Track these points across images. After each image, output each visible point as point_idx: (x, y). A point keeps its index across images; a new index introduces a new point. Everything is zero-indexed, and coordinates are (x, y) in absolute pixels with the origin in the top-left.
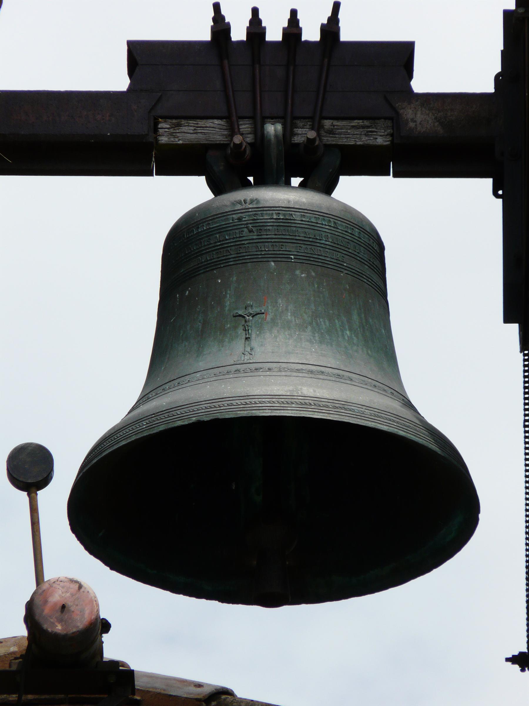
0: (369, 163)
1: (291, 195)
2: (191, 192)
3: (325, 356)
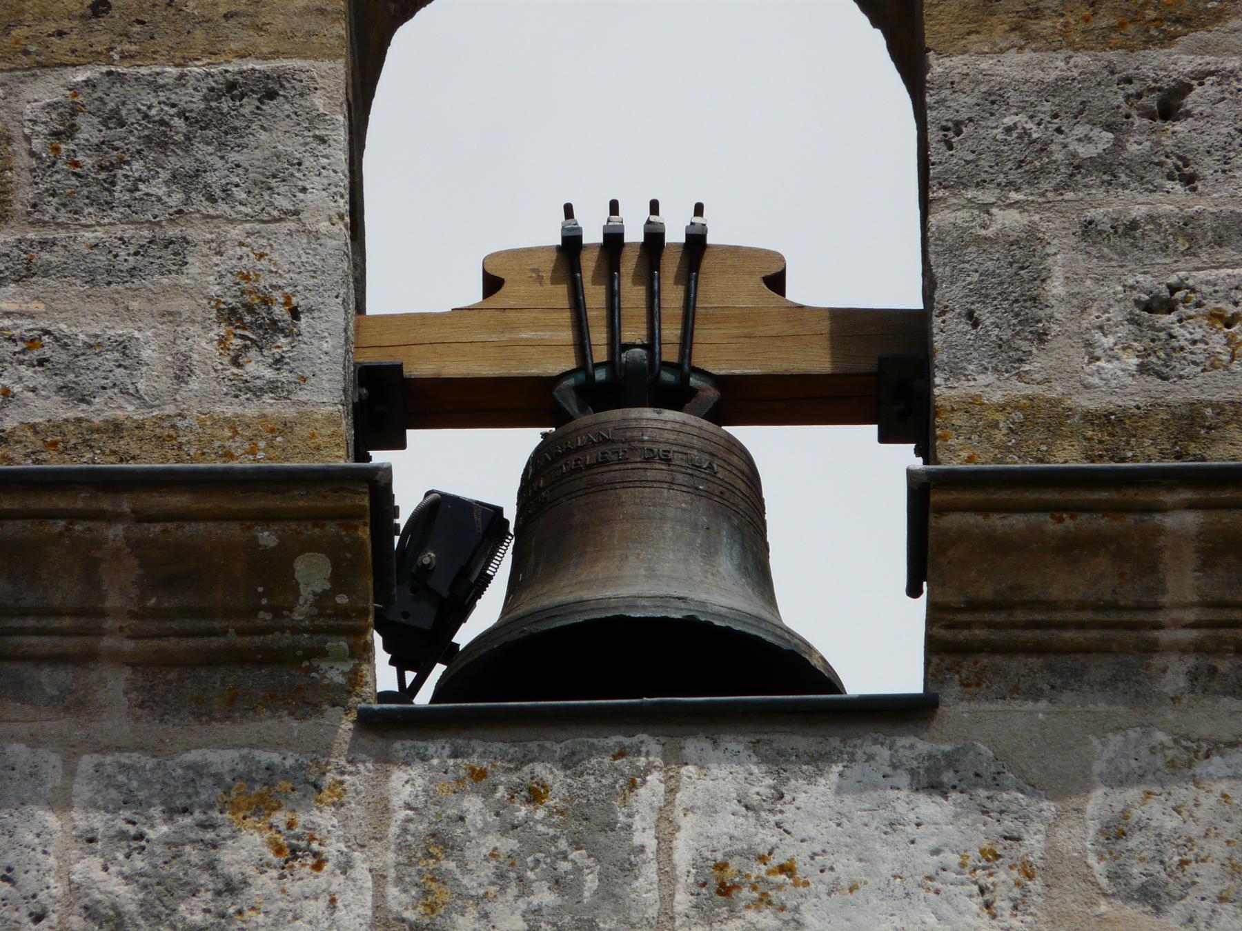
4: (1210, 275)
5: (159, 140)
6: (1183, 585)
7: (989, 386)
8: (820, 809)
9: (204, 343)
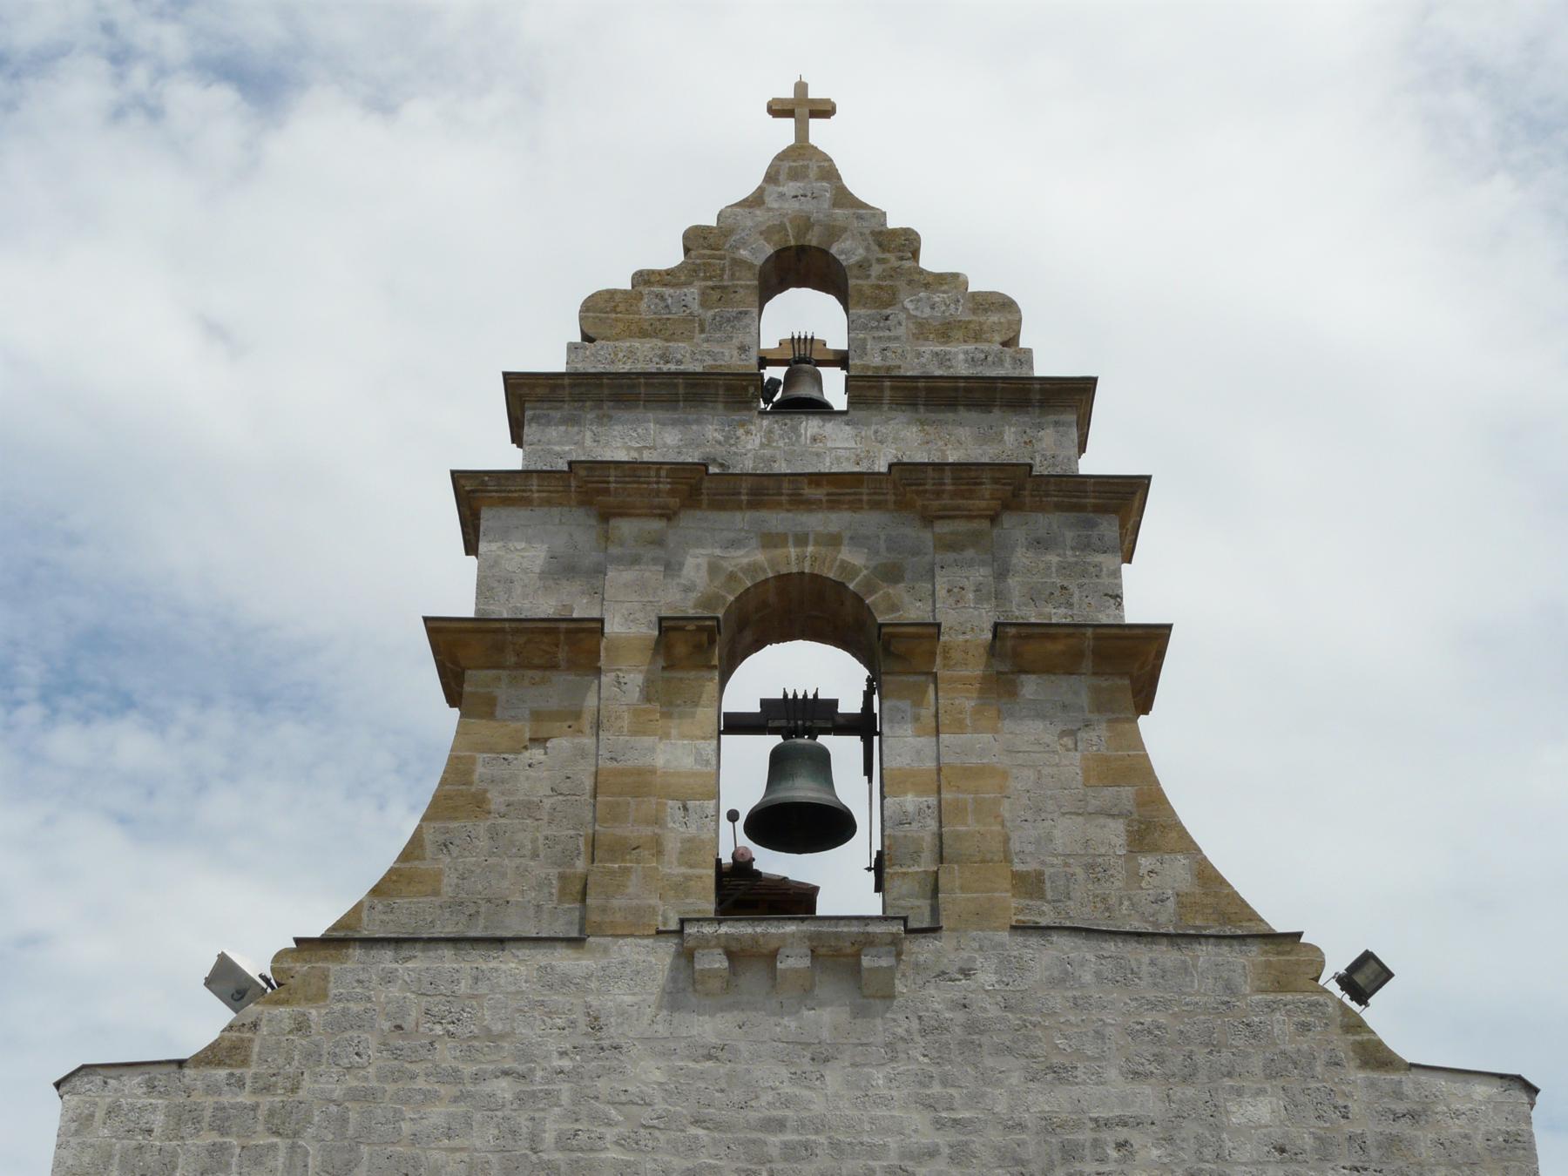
0: (826, 732)
1: (805, 740)
2: (777, 740)
3: (811, 784)
4: (893, 345)
5: (729, 320)
6: (887, 393)
7: (857, 362)
8: (830, 428)
9: (735, 353)
